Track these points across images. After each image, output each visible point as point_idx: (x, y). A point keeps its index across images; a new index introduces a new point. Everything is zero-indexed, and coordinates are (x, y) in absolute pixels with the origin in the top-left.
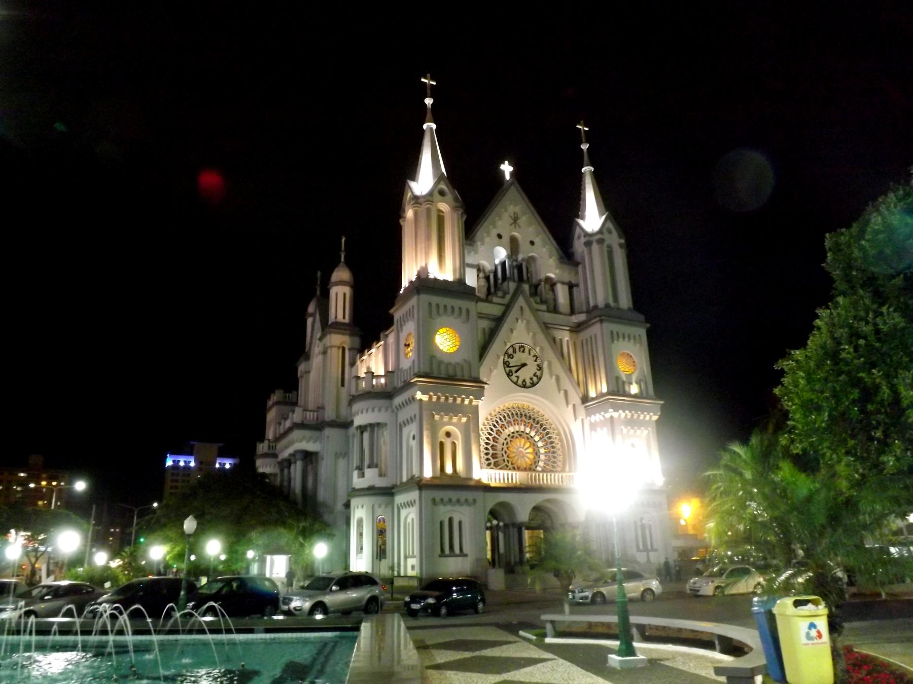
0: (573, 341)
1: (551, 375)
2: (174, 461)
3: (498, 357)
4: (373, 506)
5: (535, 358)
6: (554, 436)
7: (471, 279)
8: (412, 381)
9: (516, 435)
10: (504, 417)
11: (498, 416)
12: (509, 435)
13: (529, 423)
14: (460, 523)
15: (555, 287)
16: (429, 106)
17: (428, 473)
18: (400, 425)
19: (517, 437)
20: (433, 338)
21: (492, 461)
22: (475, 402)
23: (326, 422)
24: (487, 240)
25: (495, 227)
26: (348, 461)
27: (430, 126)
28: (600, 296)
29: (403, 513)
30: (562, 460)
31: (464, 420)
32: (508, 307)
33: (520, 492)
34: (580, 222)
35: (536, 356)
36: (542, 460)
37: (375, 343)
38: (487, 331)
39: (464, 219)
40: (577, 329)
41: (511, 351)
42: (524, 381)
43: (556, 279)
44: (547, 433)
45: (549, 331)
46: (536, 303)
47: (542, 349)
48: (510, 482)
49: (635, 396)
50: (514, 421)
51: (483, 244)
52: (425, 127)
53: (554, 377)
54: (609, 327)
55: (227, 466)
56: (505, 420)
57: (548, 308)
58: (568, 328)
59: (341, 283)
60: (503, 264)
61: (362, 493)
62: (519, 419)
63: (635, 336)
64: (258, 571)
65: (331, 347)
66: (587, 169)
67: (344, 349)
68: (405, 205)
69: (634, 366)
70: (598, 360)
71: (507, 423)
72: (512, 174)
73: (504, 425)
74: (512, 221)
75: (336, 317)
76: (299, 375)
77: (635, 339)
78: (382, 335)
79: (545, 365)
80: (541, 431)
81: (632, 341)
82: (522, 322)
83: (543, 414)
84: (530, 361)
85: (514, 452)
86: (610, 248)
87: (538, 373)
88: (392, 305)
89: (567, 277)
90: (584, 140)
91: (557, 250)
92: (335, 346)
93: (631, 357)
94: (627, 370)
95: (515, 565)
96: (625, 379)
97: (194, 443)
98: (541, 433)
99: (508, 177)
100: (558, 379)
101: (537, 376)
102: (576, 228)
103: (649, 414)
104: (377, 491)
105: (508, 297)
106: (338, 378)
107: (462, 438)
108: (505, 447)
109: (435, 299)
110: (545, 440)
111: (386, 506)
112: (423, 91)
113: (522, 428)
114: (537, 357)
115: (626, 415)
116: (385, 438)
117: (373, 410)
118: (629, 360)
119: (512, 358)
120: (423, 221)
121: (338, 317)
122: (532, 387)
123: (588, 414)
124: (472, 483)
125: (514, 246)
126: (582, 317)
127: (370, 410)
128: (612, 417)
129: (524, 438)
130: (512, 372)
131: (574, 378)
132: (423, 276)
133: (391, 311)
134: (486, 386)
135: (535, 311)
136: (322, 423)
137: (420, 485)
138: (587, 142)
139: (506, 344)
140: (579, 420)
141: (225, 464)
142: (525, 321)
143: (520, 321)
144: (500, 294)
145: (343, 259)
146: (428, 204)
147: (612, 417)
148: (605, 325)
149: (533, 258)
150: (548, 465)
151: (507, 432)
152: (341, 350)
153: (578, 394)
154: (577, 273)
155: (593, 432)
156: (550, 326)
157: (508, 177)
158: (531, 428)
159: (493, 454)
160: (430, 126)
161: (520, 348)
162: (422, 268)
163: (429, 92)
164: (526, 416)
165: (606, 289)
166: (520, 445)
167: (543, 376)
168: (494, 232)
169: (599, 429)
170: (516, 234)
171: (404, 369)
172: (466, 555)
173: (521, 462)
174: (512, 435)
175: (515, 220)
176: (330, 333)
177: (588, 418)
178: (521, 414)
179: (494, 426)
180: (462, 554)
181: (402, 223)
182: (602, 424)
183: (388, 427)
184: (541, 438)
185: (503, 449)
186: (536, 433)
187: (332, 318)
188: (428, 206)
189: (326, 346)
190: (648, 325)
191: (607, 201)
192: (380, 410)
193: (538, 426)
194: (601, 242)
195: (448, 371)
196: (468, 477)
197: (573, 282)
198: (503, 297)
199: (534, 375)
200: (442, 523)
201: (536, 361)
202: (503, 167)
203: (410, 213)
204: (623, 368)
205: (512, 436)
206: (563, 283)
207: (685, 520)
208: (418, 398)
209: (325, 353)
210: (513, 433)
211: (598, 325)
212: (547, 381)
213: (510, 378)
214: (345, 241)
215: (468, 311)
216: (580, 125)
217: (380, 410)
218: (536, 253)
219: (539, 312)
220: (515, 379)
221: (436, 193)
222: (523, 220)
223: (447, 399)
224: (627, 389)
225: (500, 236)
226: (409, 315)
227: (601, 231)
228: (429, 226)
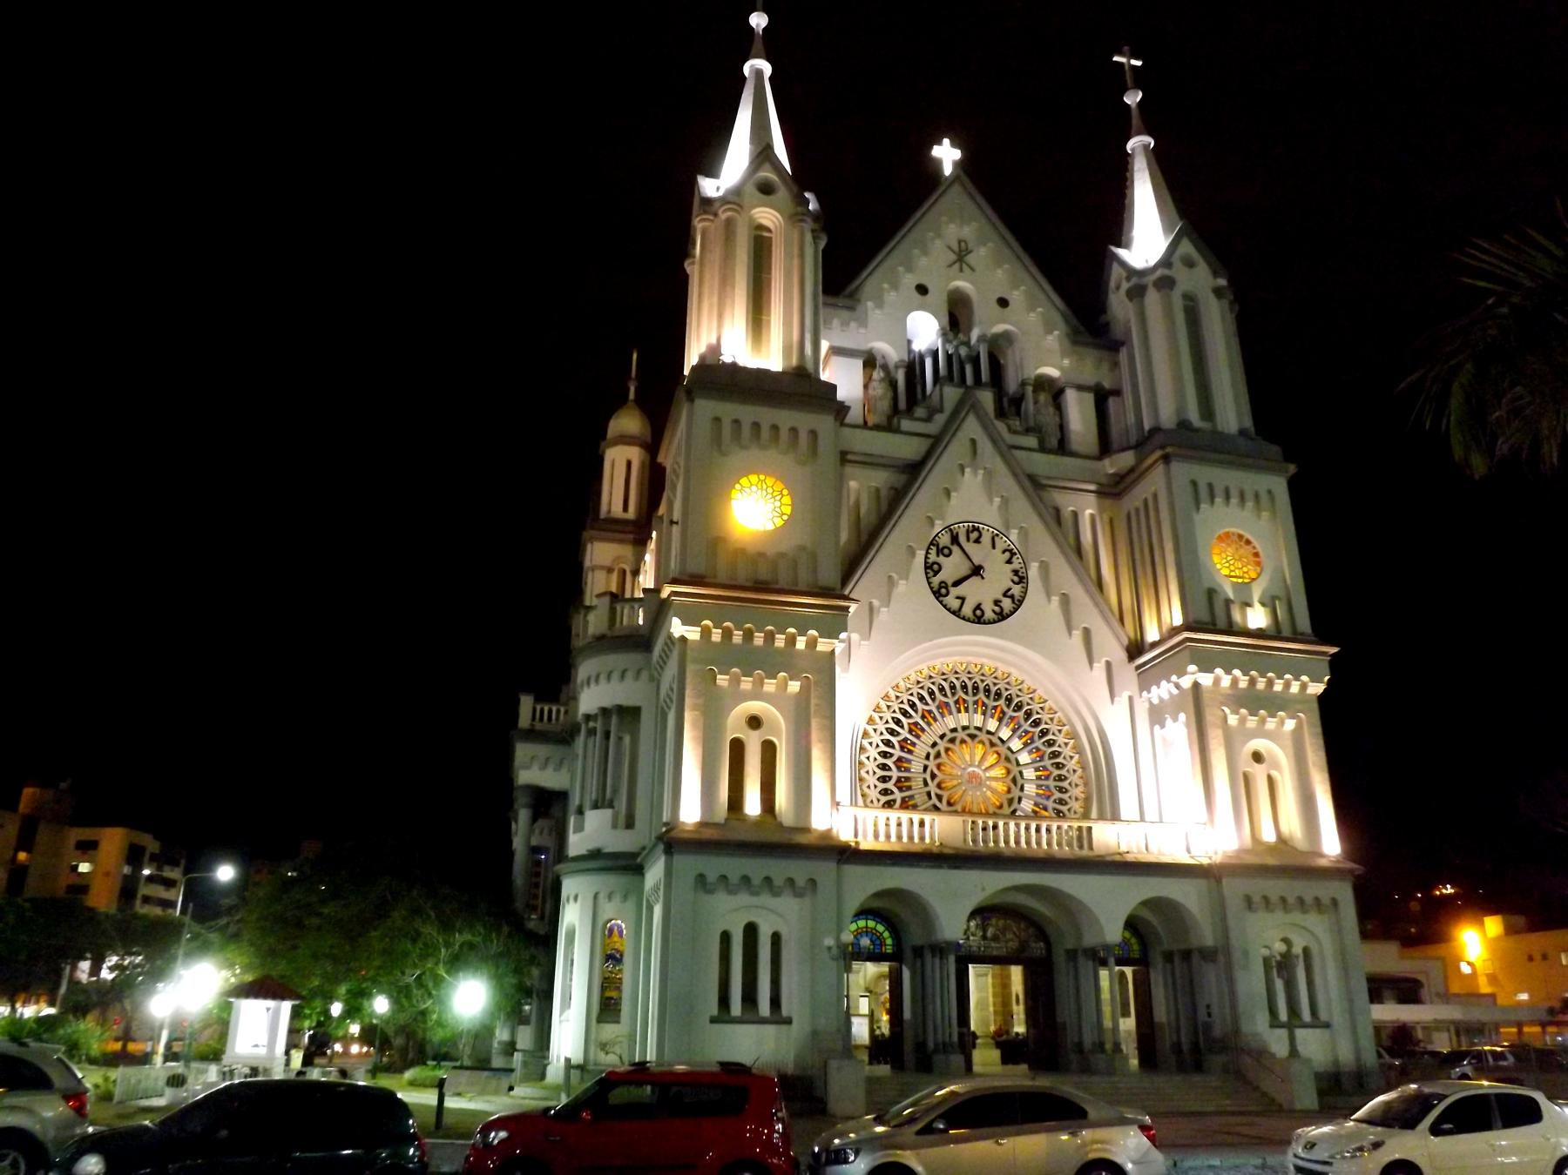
0: (1106, 518)
1: (1049, 595)
3: (912, 552)
4: (596, 897)
5: (1007, 555)
6: (1061, 739)
7: (846, 379)
9: (961, 735)
11: (915, 690)
12: (942, 737)
13: (995, 708)
14: (776, 939)
17: (690, 812)
19: (963, 741)
21: (898, 796)
22: (823, 645)
24: (891, 297)
25: (910, 269)
27: (758, 66)
31: (794, 686)
32: (936, 444)
33: (940, 867)
34: (1122, 253)
36: (1029, 797)
38: (884, 493)
39: (822, 244)
40: (1113, 489)
42: (978, 607)
43: (1063, 380)
44: (1044, 733)
45: (1045, 495)
46: (1012, 431)
47: (1024, 533)
49: (1259, 634)
50: (957, 702)
51: (880, 304)
52: (1130, 146)
54: (1183, 471)
57: (1042, 442)
58: (1092, 487)
59: (625, 440)
62: (970, 699)
64: (1513, 1027)
69: (1258, 564)
70: (1163, 557)
71: (938, 707)
72: (960, 166)
73: (930, 712)
74: (953, 257)
79: (1033, 572)
80: (1026, 726)
82: (975, 473)
83: (1033, 687)
85: (953, 776)
87: (1016, 590)
91: (1063, 315)
92: (602, 568)
93: (1248, 542)
94: (1238, 573)
95: (936, 1051)
96: (1231, 595)
101: (1012, 597)
102: (1111, 265)
103: (1297, 679)
104: (609, 863)
105: (940, 419)
108: (932, 764)
110: (1038, 749)
111: (625, 898)
112: (1118, 80)
113: (978, 720)
114: (1013, 554)
115: (1235, 681)
117: (623, 676)
118: (1242, 551)
122: (999, 621)
123: (1144, 686)
124: (802, 839)
125: (956, 318)
126: (1126, 459)
127: (616, 676)
128: (1196, 685)
129: (982, 742)
131: (1107, 601)
135: (1006, 451)
138: (1137, 86)
139: (931, 522)
143: (968, 470)
144: (920, 412)
145: (632, 395)
146: (729, 209)
147: (1196, 685)
149: (1007, 337)
150: (1045, 809)
151: (938, 728)
153: (1118, 638)
154: (1115, 365)
156: (1045, 482)
158: (1000, 720)
159: (899, 780)
161: (968, 532)
170: (962, 284)
172: (788, 1021)
173: (973, 797)
174: (950, 735)
175: (961, 255)
179: (905, 713)
180: (778, 1016)
181: (688, 269)
185: (926, 768)
190: (1292, 468)
196: (800, 825)
197: (1107, 384)
199: (1005, 595)
200: (726, 938)
201: (1009, 562)
202: (937, 151)
204: (1225, 567)
206: (1080, 388)
207: (1469, 963)
208: (677, 635)
210: (954, 730)
212: (1039, 607)
213: (941, 602)
215: (813, 434)
216: (1121, 54)
219: (1018, 453)
220: (955, 604)
223: (749, 636)
224: (1237, 616)
225: (922, 290)
227: (1166, 262)
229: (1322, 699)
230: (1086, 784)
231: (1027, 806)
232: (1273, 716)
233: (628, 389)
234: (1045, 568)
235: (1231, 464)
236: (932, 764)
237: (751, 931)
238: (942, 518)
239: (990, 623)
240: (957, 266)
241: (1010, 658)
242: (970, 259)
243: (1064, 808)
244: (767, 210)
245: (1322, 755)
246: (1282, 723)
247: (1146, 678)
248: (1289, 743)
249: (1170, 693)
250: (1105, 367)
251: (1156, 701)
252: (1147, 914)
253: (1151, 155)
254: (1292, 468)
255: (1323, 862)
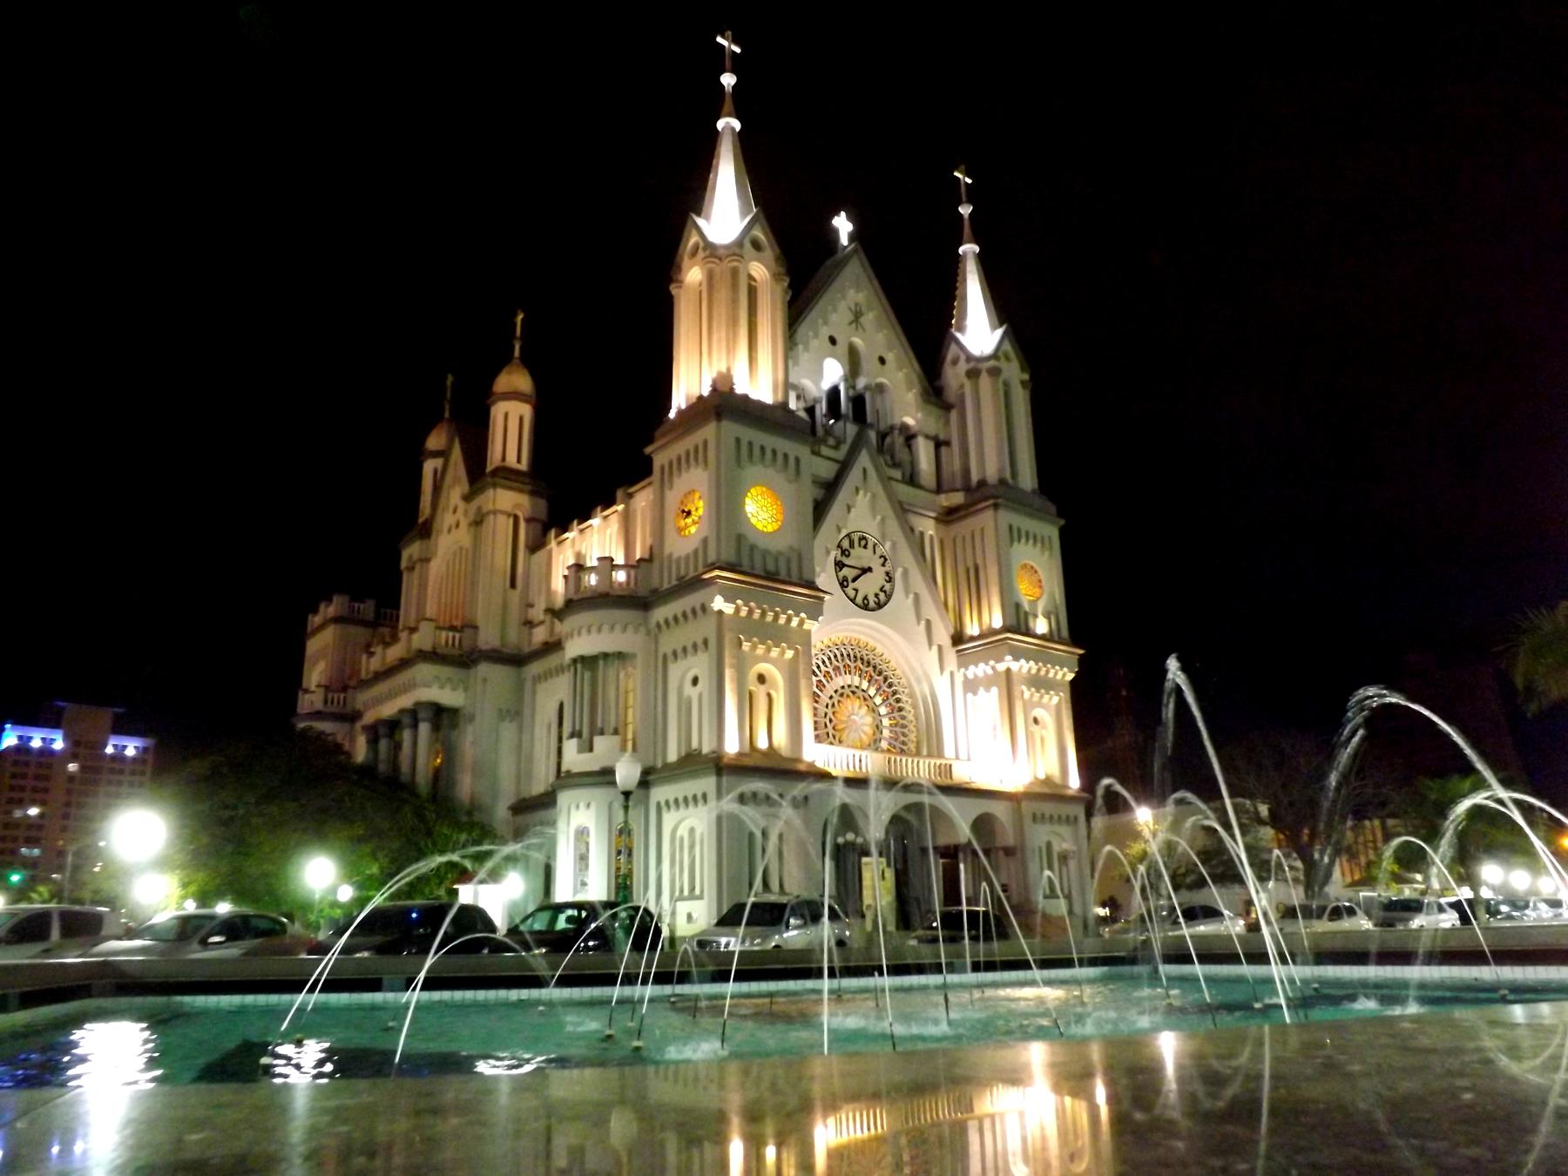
1: (907, 593)
2: (20, 738)
3: (828, 552)
5: (883, 559)
6: (904, 698)
8: (706, 576)
9: (847, 691)
10: (829, 659)
11: (821, 656)
12: (836, 691)
15: (913, 442)
16: (728, 89)
18: (665, 657)
19: (848, 696)
20: (741, 505)
23: (480, 651)
24: (814, 343)
25: (826, 323)
26: (520, 730)
28: (989, 464)
29: (669, 819)
30: (915, 739)
31: (789, 654)
32: (844, 467)
35: (884, 557)
36: (885, 739)
37: (599, 509)
39: (788, 298)
40: (949, 516)
41: (846, 544)
42: (865, 598)
43: (916, 429)
44: (895, 693)
48: (858, 769)
49: (1042, 637)
51: (806, 349)
52: (720, 124)
53: (911, 596)
54: (1007, 517)
55: (130, 752)
56: (831, 663)
58: (933, 514)
60: (834, 393)
61: (590, 780)
62: (852, 665)
63: (1043, 538)
65: (495, 512)
66: (969, 249)
67: (516, 518)
68: (682, 260)
69: (1041, 587)
74: (851, 317)
75: (504, 459)
76: (404, 564)
77: (1043, 543)
78: (620, 494)
79: (898, 575)
81: (1039, 545)
82: (865, 495)
84: (875, 563)
85: (843, 722)
86: (1006, 384)
88: (651, 441)
89: (932, 431)
90: (964, 198)
91: (919, 376)
92: (502, 512)
93: (1036, 572)
94: (1029, 593)
97: (64, 704)
98: (884, 691)
99: (844, 240)
100: (917, 598)
101: (885, 592)
102: (950, 344)
103: (1053, 668)
105: (845, 448)
106: (505, 572)
107: (785, 686)
108: (830, 711)
109: (748, 434)
112: (719, 62)
114: (886, 560)
116: (630, 684)
117: (612, 628)
119: (848, 556)
120: (722, 295)
121: (508, 459)
124: (802, 767)
126: (958, 498)
127: (584, 631)
128: (1008, 670)
130: (847, 581)
131: (939, 597)
132: (723, 388)
133: (648, 450)
134: (827, 597)
135: (886, 481)
136: (472, 653)
137: (720, 767)
138: (969, 201)
139: (839, 530)
140: (947, 673)
141: (125, 747)
142: (869, 494)
143: (861, 492)
147: (1008, 670)
148: (1002, 513)
151: (830, 688)
152: (511, 520)
154: (947, 423)
155: (970, 695)
157: (844, 240)
160: (728, 124)
162: (720, 374)
163: (728, 63)
164: (862, 659)
165: (1000, 454)
166: (853, 709)
167: (894, 595)
168: (825, 332)
169: (981, 691)
171: (675, 556)
174: (840, 691)
175: (857, 316)
176: (495, 486)
177: (963, 670)
178: (855, 657)
182: (988, 682)
183: (639, 661)
184: (884, 701)
185: (826, 714)
186: (878, 690)
187: (494, 458)
188: (735, 264)
189: (485, 510)
191: (1003, 307)
192: (624, 629)
193: (881, 678)
194: (995, 372)
195: (765, 564)
196: (795, 756)
197: (942, 437)
198: (836, 447)
200: (1040, 849)
201: (883, 565)
203: (693, 275)
204: (1025, 591)
205: (841, 693)
206: (927, 437)
208: (716, 609)
209: (478, 522)
210: (843, 687)
211: (989, 514)
214: (523, 320)
217: (624, 629)
218: (888, 379)
221: (748, 245)
222: (869, 318)
223: (763, 614)
224: (1031, 624)
225: (833, 341)
226: (697, 456)
227: (995, 356)
228: (735, 301)
229: (1072, 682)
230: (918, 731)
231: (884, 745)
232: (777, 646)
233: (513, 347)
234: (906, 573)
235: (1031, 516)
236: (830, 711)
237: (692, 831)
238: (846, 528)
239: (885, 604)
240: (854, 325)
241: (875, 634)
242: (862, 320)
243: (905, 748)
244: (763, 268)
245: (1071, 721)
246: (1051, 699)
247: (964, 660)
248: (1053, 712)
249: (985, 672)
250: (941, 425)
251: (970, 676)
252: (904, 814)
253: (737, 139)
254: (1062, 522)
255: (1070, 792)
